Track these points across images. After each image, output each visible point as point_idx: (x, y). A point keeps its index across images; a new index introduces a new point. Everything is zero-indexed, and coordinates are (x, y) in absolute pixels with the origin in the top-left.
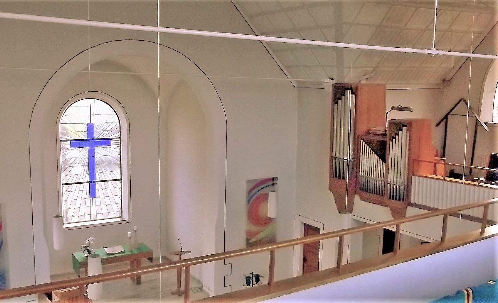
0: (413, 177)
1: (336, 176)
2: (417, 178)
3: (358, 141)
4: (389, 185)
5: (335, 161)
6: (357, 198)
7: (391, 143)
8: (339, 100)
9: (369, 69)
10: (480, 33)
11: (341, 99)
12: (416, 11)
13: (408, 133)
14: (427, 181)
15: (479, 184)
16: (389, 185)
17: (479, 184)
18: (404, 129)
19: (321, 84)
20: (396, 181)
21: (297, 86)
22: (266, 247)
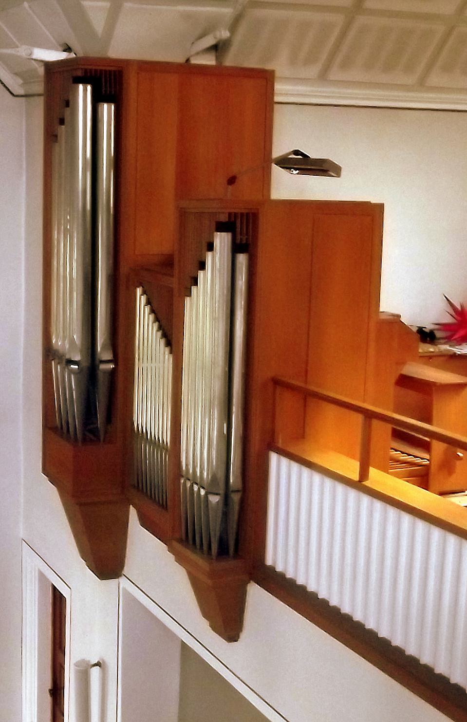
21: (21, 92)
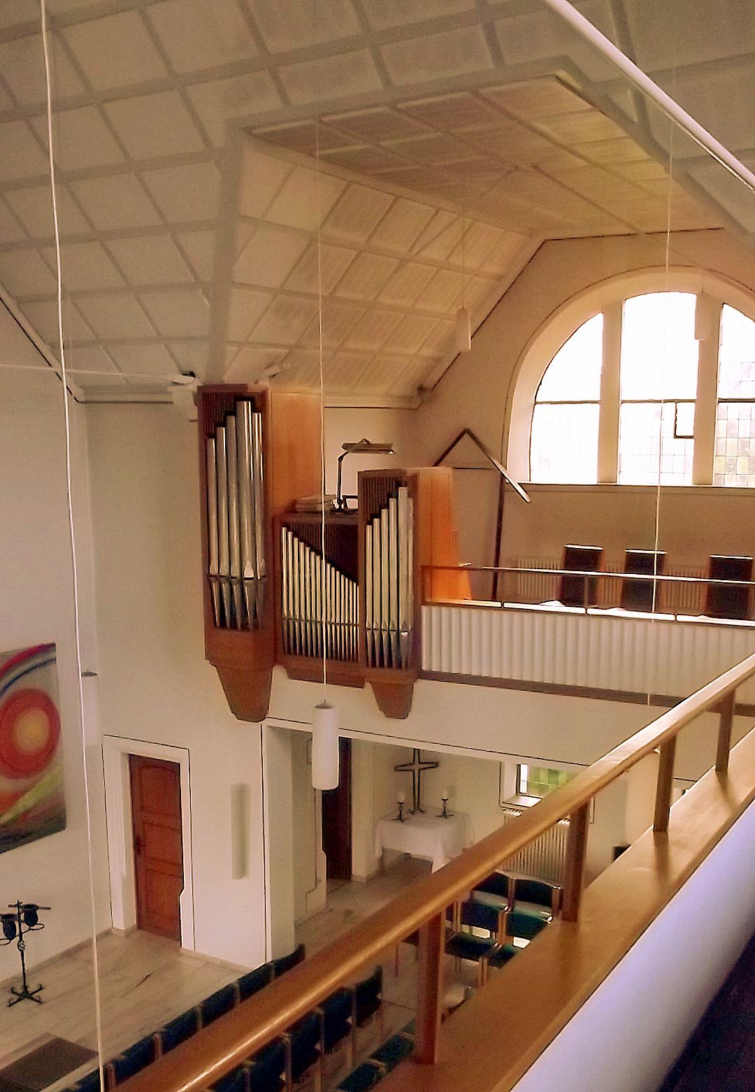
0: (424, 609)
1: (223, 624)
2: (435, 609)
3: (273, 529)
4: (369, 633)
5: (227, 585)
6: (279, 674)
7: (369, 528)
8: (219, 429)
9: (279, 350)
10: (499, 278)
11: (224, 424)
12: (395, 202)
13: (411, 501)
14: (491, 618)
15: (503, 605)
16: (369, 633)
17: (503, 605)
18: (403, 492)
19: (162, 389)
20: (378, 621)
21: (83, 400)
22: (247, 1040)
